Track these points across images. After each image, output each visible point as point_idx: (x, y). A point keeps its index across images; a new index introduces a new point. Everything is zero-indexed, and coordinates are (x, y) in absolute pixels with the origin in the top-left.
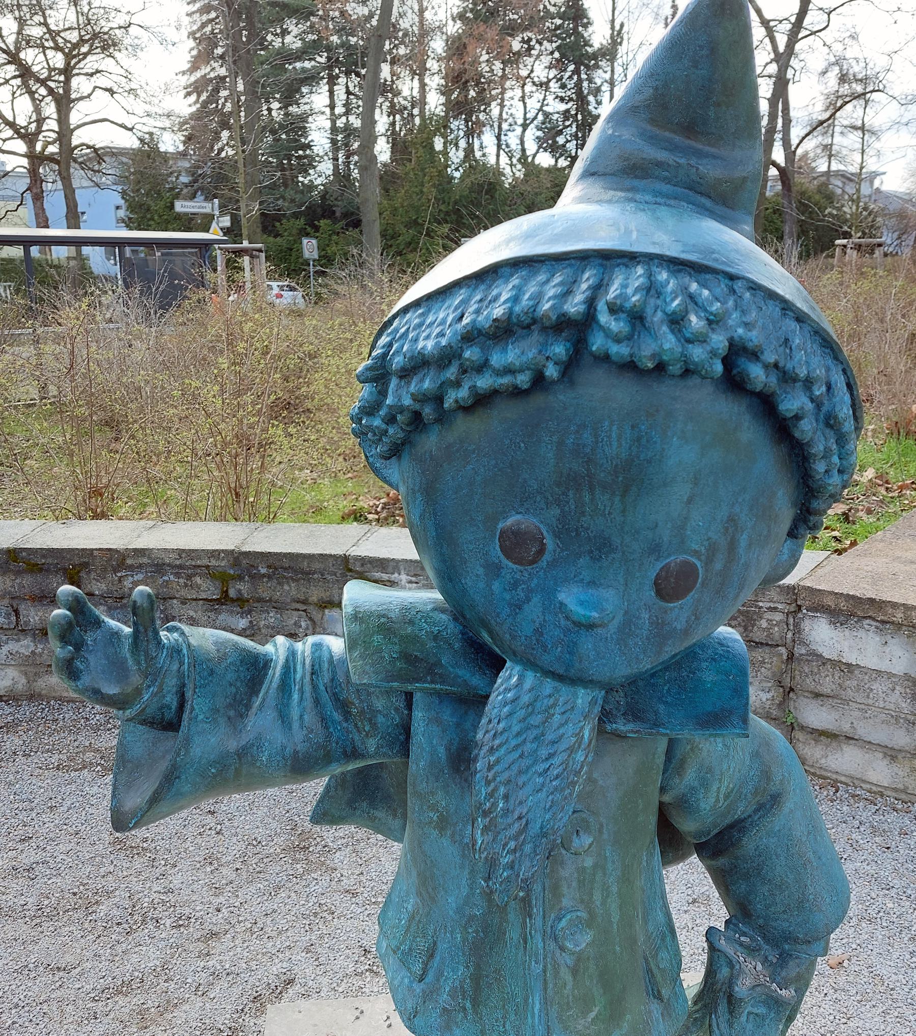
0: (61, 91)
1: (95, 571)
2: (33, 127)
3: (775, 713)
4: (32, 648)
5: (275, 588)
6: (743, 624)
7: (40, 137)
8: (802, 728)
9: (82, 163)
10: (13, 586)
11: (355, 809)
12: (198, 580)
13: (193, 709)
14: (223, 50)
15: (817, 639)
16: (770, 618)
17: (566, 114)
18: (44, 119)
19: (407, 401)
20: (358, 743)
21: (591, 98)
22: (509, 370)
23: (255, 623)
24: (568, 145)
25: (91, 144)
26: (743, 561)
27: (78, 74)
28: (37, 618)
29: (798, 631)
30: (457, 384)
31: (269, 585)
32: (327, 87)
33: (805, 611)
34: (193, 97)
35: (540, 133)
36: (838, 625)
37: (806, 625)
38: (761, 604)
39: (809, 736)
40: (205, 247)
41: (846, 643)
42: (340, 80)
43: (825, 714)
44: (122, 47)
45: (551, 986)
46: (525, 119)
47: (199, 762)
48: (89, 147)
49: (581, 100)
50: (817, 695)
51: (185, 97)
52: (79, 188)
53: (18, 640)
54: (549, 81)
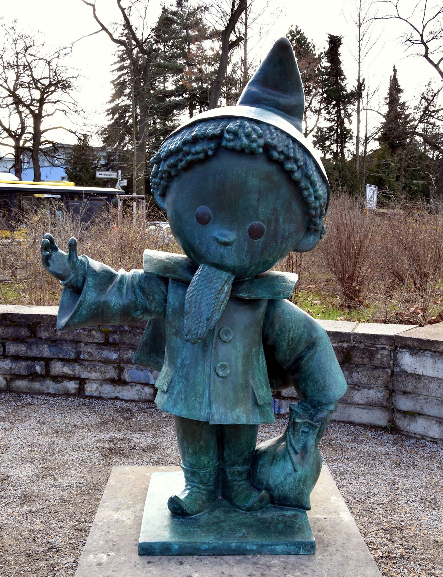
0: (37, 112)
1: (44, 327)
2: (19, 131)
3: (385, 403)
4: (10, 366)
5: (132, 337)
6: (369, 357)
7: (23, 138)
8: (399, 411)
9: (45, 152)
10: (3, 333)
11: (151, 356)
12: (94, 333)
13: (88, 281)
14: (130, 90)
15: (405, 363)
16: (382, 353)
17: (331, 129)
18: (26, 127)
19: (166, 168)
20: (148, 306)
21: (346, 120)
22: (197, 153)
23: (121, 356)
24: (332, 146)
25: (51, 141)
26: (282, 227)
27: (47, 103)
28: (14, 350)
29: (395, 359)
30: (181, 160)
31: (129, 336)
32: (188, 111)
33: (398, 349)
34: (111, 116)
35: (315, 139)
36: (414, 355)
37: (399, 356)
38: (377, 346)
39: (401, 415)
40: (111, 195)
41: (418, 364)
42: (197, 107)
43: (408, 402)
44: (73, 88)
45: (212, 386)
46: (306, 130)
47: (89, 302)
48: (50, 142)
49: (340, 122)
50: (405, 393)
51: (107, 116)
52: (42, 167)
53: (4, 361)
54: (321, 109)
